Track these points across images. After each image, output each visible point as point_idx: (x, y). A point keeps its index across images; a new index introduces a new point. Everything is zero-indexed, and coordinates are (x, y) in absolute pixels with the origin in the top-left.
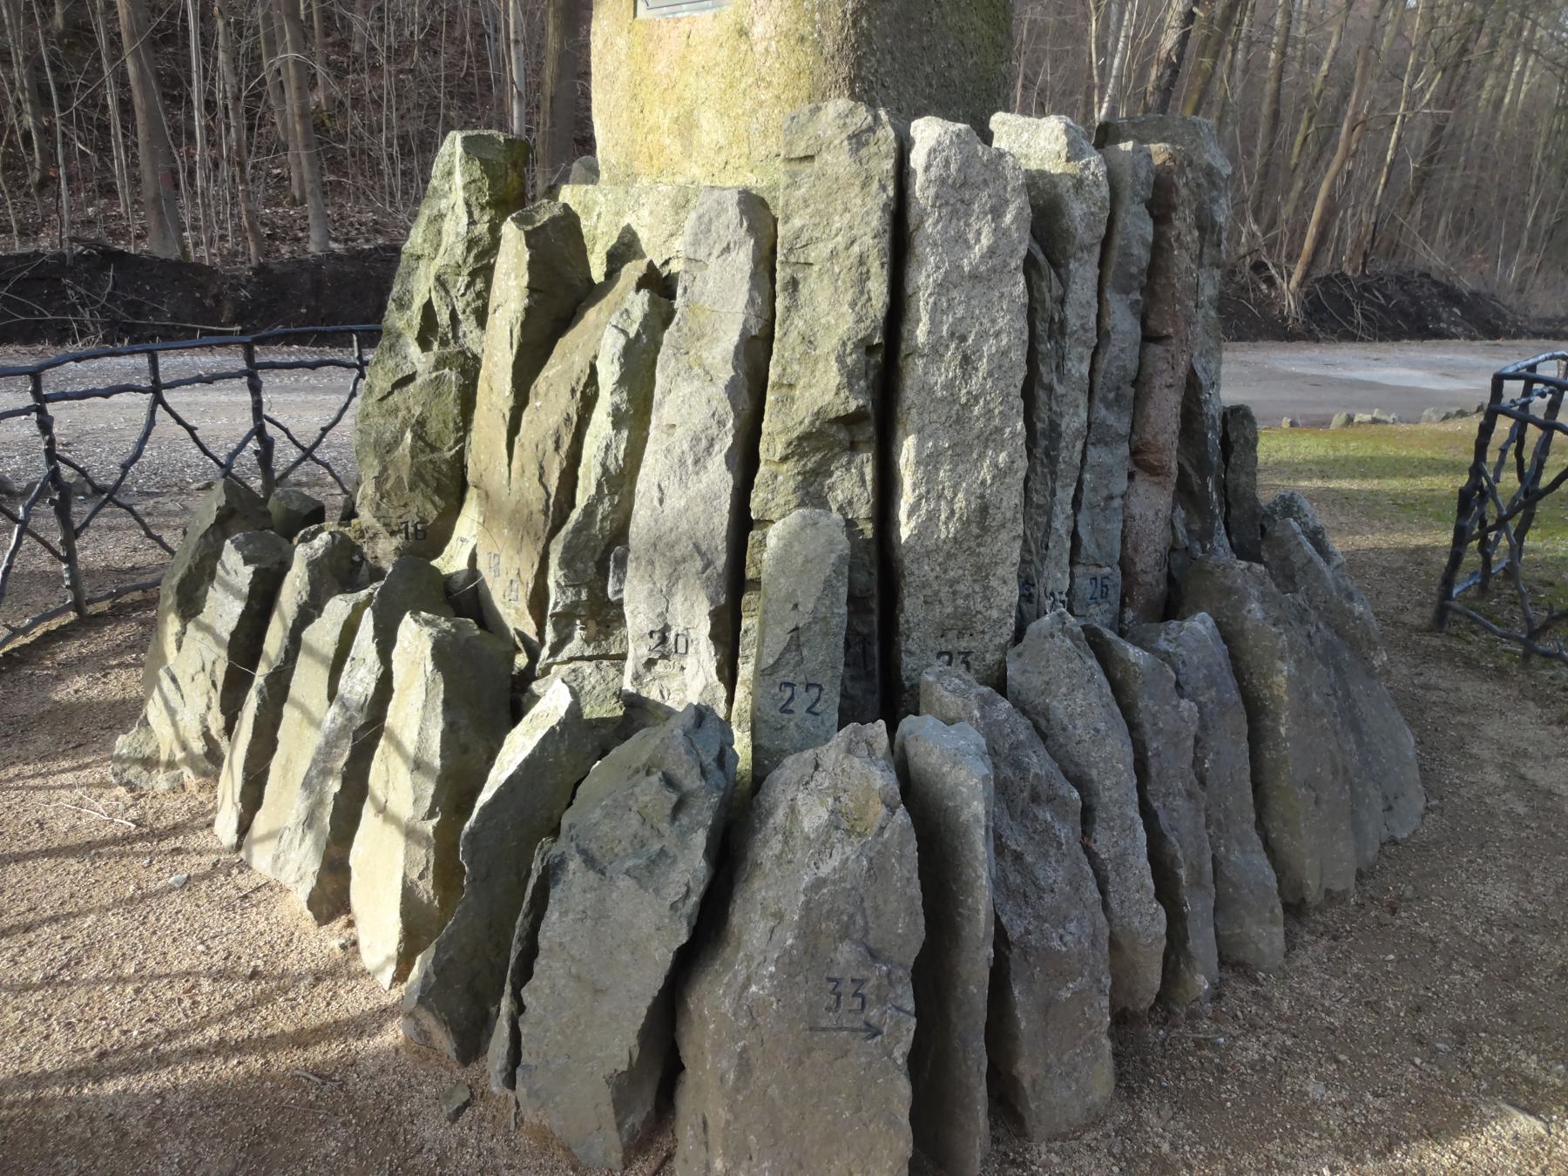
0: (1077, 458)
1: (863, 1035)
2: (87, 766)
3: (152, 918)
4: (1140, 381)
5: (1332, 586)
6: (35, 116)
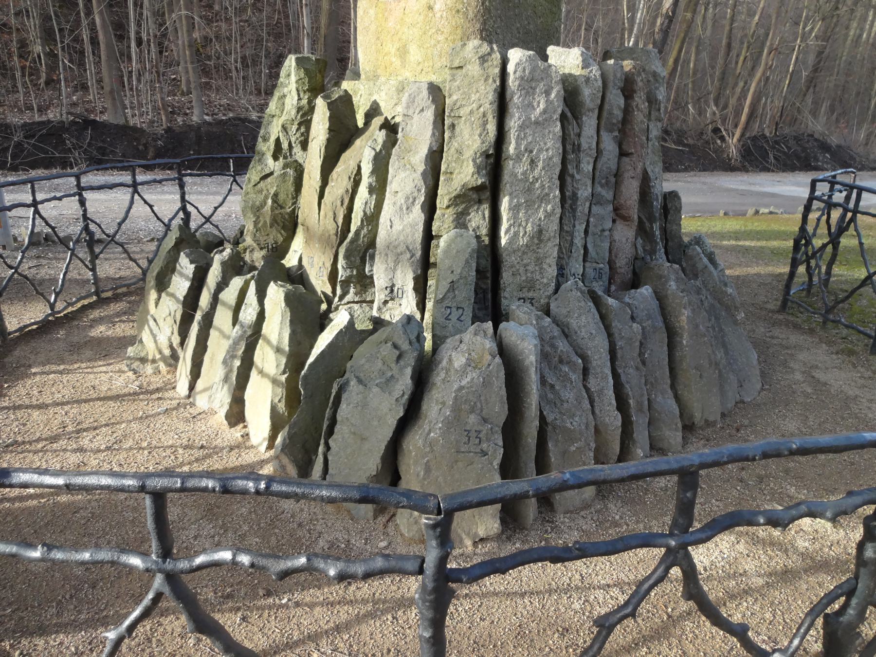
0: (587, 211)
1: (480, 455)
2: (111, 364)
3: (152, 425)
4: (618, 175)
5: (717, 279)
6: (43, 46)
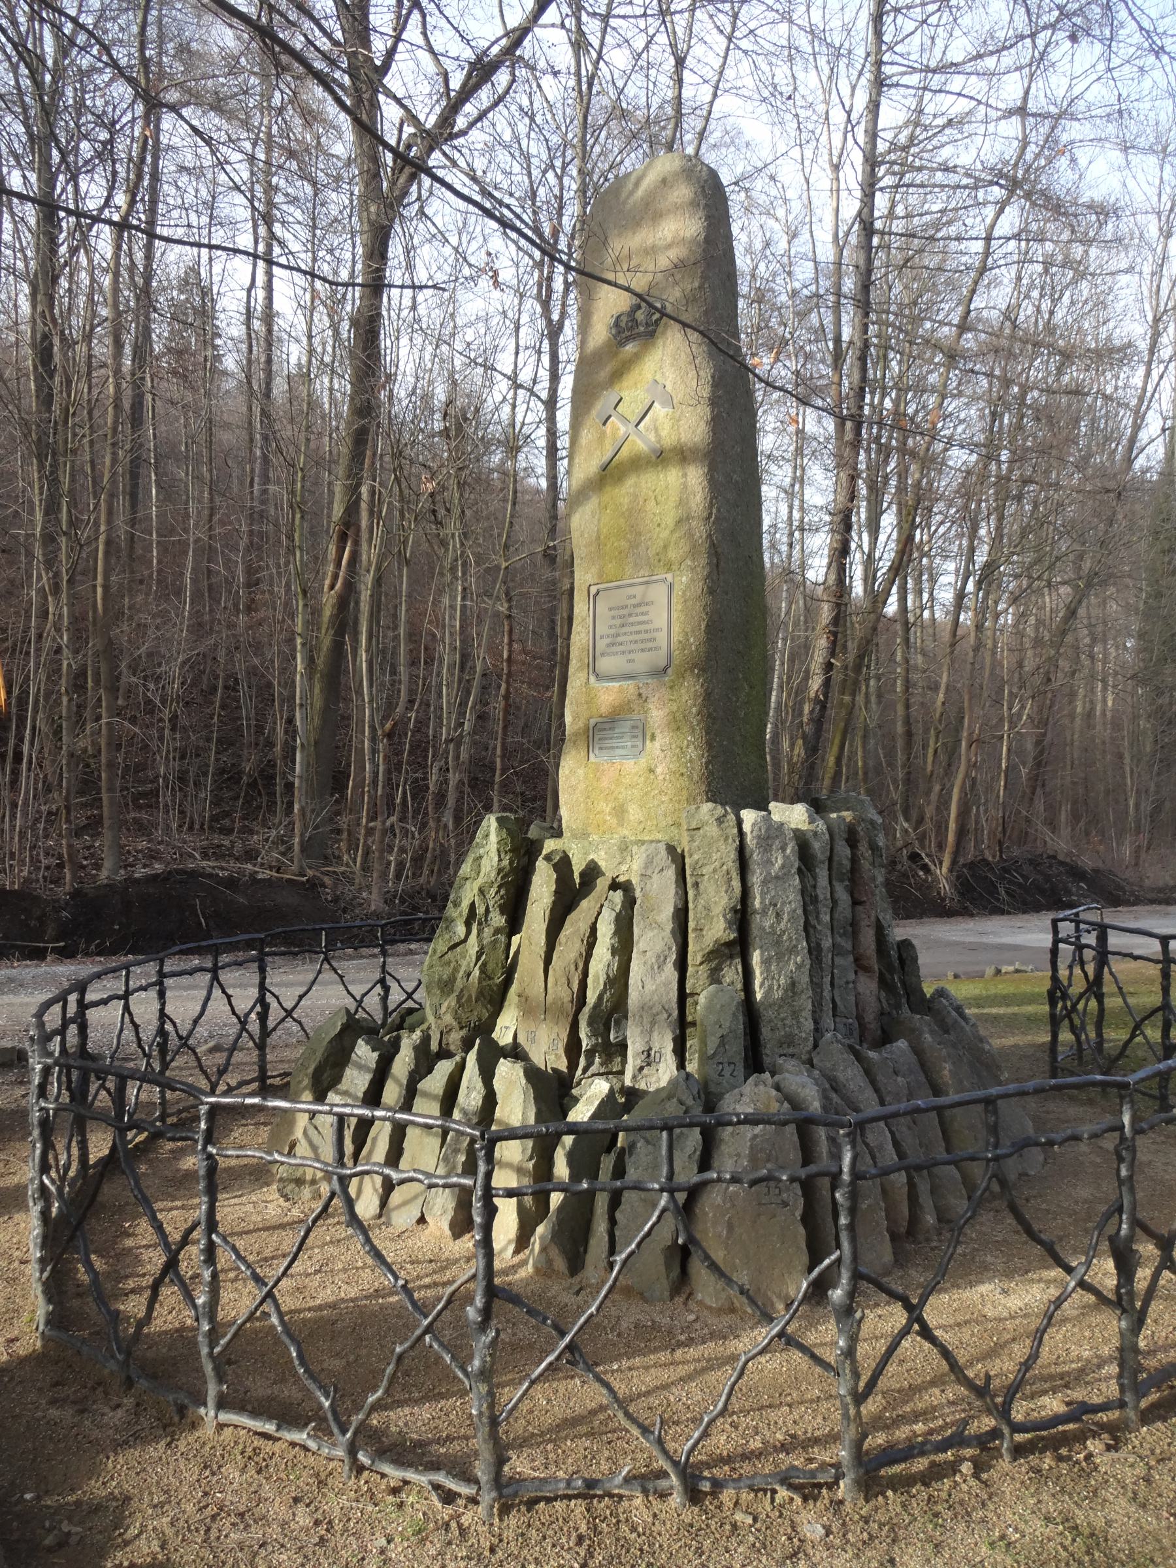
4: (854, 924)
